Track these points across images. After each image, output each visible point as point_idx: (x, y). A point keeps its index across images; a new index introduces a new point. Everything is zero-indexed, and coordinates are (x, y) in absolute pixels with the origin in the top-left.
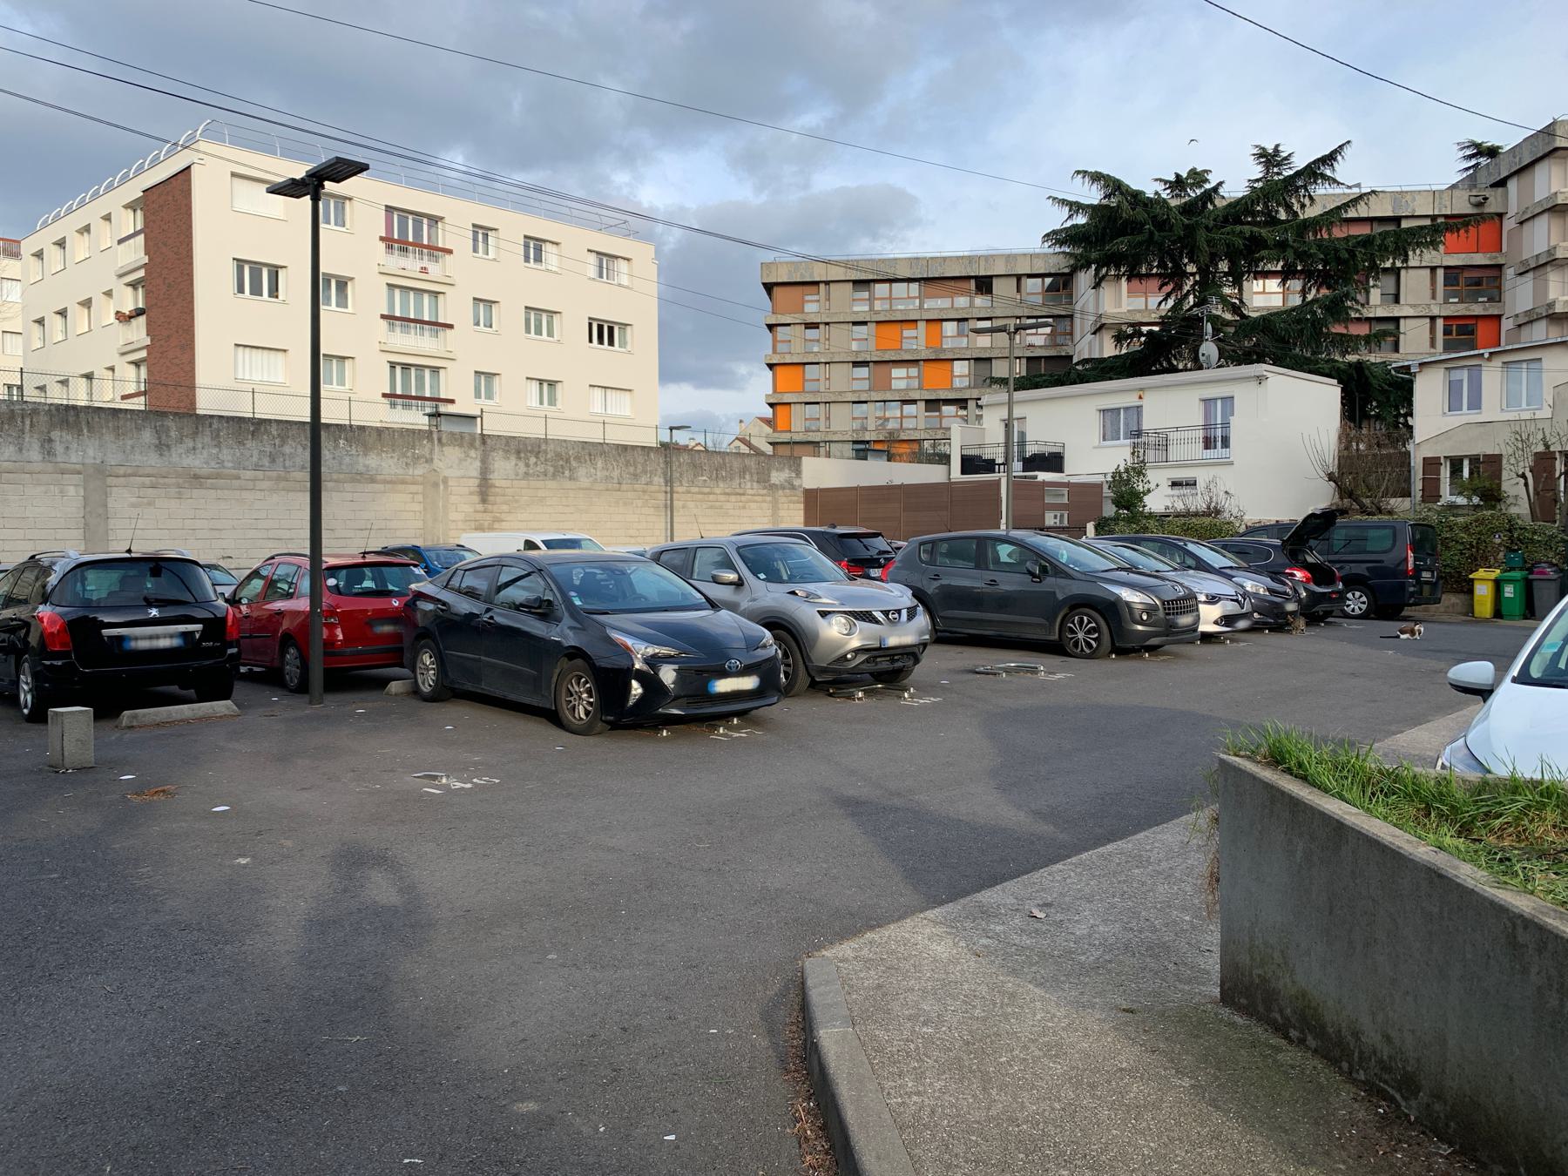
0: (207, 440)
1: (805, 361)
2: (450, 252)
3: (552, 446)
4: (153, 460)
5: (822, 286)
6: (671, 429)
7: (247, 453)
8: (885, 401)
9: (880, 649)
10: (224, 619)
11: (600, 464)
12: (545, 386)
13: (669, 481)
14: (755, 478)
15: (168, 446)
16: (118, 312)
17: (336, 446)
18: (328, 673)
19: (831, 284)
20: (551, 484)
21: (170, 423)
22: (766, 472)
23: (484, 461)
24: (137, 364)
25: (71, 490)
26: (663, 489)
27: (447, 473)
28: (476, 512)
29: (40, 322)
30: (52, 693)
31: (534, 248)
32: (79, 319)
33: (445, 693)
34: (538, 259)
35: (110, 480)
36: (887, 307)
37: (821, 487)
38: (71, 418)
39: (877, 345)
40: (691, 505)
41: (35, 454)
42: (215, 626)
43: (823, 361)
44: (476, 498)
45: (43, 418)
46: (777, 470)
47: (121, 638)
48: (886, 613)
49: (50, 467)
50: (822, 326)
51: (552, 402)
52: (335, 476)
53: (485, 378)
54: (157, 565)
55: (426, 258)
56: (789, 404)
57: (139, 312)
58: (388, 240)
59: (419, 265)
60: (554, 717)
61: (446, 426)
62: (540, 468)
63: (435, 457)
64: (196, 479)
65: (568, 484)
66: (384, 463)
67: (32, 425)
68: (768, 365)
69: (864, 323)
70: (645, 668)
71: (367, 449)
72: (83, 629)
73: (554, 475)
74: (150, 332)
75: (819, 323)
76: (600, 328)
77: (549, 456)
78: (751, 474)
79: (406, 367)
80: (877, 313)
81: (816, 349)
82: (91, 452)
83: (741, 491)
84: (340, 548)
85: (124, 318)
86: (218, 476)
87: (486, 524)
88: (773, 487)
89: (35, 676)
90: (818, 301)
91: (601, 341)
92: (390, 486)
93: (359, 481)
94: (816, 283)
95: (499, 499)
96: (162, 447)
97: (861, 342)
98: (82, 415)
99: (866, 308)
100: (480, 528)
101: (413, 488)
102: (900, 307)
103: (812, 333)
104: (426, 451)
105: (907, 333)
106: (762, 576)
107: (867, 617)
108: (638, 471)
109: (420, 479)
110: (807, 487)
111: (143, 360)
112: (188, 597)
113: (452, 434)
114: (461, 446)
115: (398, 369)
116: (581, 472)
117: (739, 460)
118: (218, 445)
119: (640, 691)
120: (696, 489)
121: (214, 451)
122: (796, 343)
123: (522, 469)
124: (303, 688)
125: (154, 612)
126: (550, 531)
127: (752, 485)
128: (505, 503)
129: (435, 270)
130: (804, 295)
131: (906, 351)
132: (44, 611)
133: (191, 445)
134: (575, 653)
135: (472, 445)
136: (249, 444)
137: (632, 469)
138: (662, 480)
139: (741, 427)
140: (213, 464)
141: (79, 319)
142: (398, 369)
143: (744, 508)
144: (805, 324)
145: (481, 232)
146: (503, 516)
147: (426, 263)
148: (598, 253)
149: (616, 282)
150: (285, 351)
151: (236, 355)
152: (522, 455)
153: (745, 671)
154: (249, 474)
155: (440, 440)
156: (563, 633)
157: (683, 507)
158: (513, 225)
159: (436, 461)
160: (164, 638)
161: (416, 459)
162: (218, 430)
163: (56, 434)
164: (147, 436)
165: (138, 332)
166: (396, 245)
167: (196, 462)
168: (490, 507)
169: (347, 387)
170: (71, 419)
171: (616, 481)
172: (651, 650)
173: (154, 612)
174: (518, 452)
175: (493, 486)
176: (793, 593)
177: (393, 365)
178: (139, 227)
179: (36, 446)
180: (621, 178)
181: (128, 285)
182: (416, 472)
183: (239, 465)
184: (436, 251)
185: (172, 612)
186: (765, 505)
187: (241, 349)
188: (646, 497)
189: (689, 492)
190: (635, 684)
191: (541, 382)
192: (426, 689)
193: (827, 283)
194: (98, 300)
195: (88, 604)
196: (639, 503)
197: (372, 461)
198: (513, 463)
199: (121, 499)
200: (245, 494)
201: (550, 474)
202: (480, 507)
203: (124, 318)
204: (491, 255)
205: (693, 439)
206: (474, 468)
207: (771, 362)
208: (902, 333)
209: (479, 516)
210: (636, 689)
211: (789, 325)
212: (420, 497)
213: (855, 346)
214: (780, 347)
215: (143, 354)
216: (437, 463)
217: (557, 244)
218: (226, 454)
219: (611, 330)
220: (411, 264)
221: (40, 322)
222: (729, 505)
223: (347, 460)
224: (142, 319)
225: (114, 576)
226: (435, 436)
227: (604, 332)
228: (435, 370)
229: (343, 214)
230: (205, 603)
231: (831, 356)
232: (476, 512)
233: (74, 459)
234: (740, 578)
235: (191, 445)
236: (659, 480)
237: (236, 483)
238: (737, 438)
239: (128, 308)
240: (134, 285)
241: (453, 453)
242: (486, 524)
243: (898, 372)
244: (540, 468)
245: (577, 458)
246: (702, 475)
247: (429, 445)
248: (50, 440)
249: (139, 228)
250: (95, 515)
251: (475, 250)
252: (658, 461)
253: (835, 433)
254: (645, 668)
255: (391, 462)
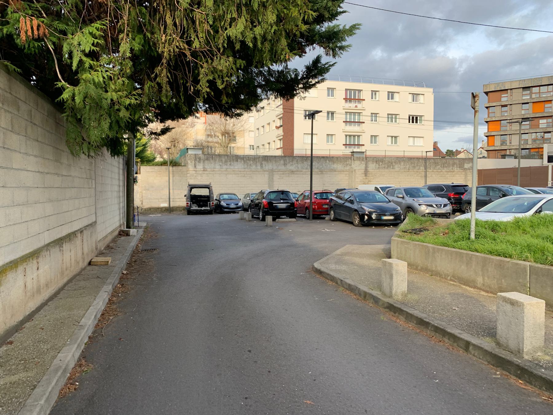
0: (295, 162)
1: (501, 119)
2: (364, 100)
3: (387, 159)
4: (283, 168)
5: (509, 91)
6: (426, 152)
7: (304, 165)
8: (536, 133)
9: (434, 213)
10: (294, 203)
11: (402, 164)
12: (393, 138)
13: (426, 168)
14: (458, 166)
15: (286, 164)
16: (276, 126)
17: (326, 162)
18: (313, 215)
19: (513, 90)
20: (386, 170)
21: (287, 159)
22: (463, 164)
23: (366, 165)
24: (280, 140)
25: (266, 175)
26: (424, 171)
27: (355, 168)
28: (363, 179)
29: (258, 129)
30: (266, 214)
31: (391, 95)
32: (267, 127)
33: (336, 219)
34: (392, 98)
35: (274, 173)
36: (538, 96)
37: (484, 169)
38: (267, 158)
39: (533, 111)
40: (434, 175)
41: (259, 167)
42: (293, 204)
43: (509, 119)
44: (363, 175)
45: (261, 159)
46: (467, 163)
47: (276, 206)
48: (437, 205)
49: (262, 170)
50: (508, 106)
51: (396, 143)
52: (325, 170)
53: (374, 138)
54: (283, 192)
55: (357, 103)
56: (494, 136)
57: (281, 126)
58: (346, 99)
59: (355, 105)
60: (351, 223)
61: (355, 155)
62: (383, 166)
63: (352, 164)
64: (293, 172)
65: (392, 170)
66: (338, 166)
67: (259, 161)
68: (486, 122)
69: (528, 103)
70: (368, 213)
71: (334, 163)
72: (270, 204)
73: (387, 168)
74: (283, 131)
75: (507, 105)
76: (413, 118)
77: (386, 162)
78: (457, 165)
79: (350, 136)
80: (534, 98)
81: (506, 115)
82: (270, 166)
83: (453, 171)
84: (317, 188)
85: (278, 128)
86: (297, 171)
87: (366, 182)
88: (465, 169)
89: (263, 213)
90: (507, 96)
91: (413, 122)
92: (339, 172)
93: (332, 171)
94: (507, 90)
95: (370, 175)
96: (285, 164)
97: (527, 111)
98: (269, 158)
99: (529, 97)
100: (364, 184)
101: (346, 173)
102: (544, 96)
103: (504, 109)
104: (350, 163)
105: (546, 106)
106: (409, 196)
107: (431, 206)
108: (415, 165)
109: (348, 170)
110: (479, 169)
111: (282, 139)
112: (288, 199)
113: (357, 157)
114: (360, 160)
115: (348, 137)
116: (396, 166)
117: (452, 160)
118: (298, 164)
119: (367, 218)
120: (436, 171)
121: (297, 165)
122: (497, 113)
123: (377, 166)
124: (309, 219)
125: (282, 201)
126: (381, 184)
127: (457, 169)
128: (372, 176)
129: (360, 106)
130: (501, 95)
131: (546, 112)
132: (264, 200)
133: (291, 163)
134: (356, 210)
135: (363, 160)
136: (305, 163)
137: (413, 165)
138: (423, 168)
139: (483, 143)
140: (296, 168)
141: (267, 127)
142: (348, 137)
143: (454, 176)
144: (502, 105)
145: (374, 93)
146: (371, 180)
147: (357, 104)
148: (412, 94)
149: (419, 102)
150: (317, 134)
151: (304, 136)
152: (378, 162)
153: (391, 215)
154: (304, 170)
155: (354, 159)
156: (355, 206)
157: (431, 176)
158: (384, 89)
159: (352, 165)
160: (283, 206)
161: (347, 165)
162: (298, 160)
163: (263, 162)
164: (282, 162)
165: (281, 131)
166: (348, 100)
167: (293, 168)
168: (368, 178)
169: (333, 143)
170: (266, 159)
171: (407, 169)
172: (370, 210)
173: (282, 201)
174: (376, 161)
175: (369, 171)
176: (414, 200)
177: (346, 136)
178: (281, 103)
179: (259, 165)
180: (440, 49)
181: (278, 119)
182: (347, 168)
183: (302, 168)
184: (360, 100)
185: (285, 201)
186: (461, 175)
187: (305, 135)
188: (418, 173)
189: (433, 172)
190: (366, 216)
191: (392, 137)
192: (332, 218)
193: (511, 89)
194: (272, 123)
195: (271, 200)
196: (416, 175)
197: (335, 166)
198: (375, 165)
199: (276, 177)
200: (304, 175)
201: (386, 168)
202: (365, 178)
203: (278, 128)
204: (377, 99)
205: (463, 148)
206: (363, 166)
207: (487, 121)
208: (544, 106)
209: (364, 180)
210: (366, 217)
211: (495, 106)
212: (348, 175)
213: (523, 112)
214: (491, 115)
215: (282, 137)
216: (353, 166)
217: (399, 93)
218: (299, 166)
219: (417, 118)
220: (352, 105)
221: (258, 129)
222: (447, 175)
223: (329, 166)
224: (282, 128)
225: (275, 194)
226: (352, 158)
227: (414, 119)
228: (359, 136)
229: (333, 93)
230: (291, 200)
231: (512, 116)
232: (363, 179)
233: (267, 168)
234: (403, 196)
235: (291, 163)
236: (422, 168)
237: (302, 173)
238: (95, 222)
239: (278, 125)
240: (280, 119)
241: (357, 163)
242: (366, 182)
243: (542, 121)
244: (383, 166)
245: (395, 162)
246: (438, 166)
247: (350, 161)
248: (262, 164)
249: (282, 146)
250: (271, 181)
251: (372, 98)
252: (422, 162)
253: (513, 146)
254: (368, 213)
255: (340, 166)
